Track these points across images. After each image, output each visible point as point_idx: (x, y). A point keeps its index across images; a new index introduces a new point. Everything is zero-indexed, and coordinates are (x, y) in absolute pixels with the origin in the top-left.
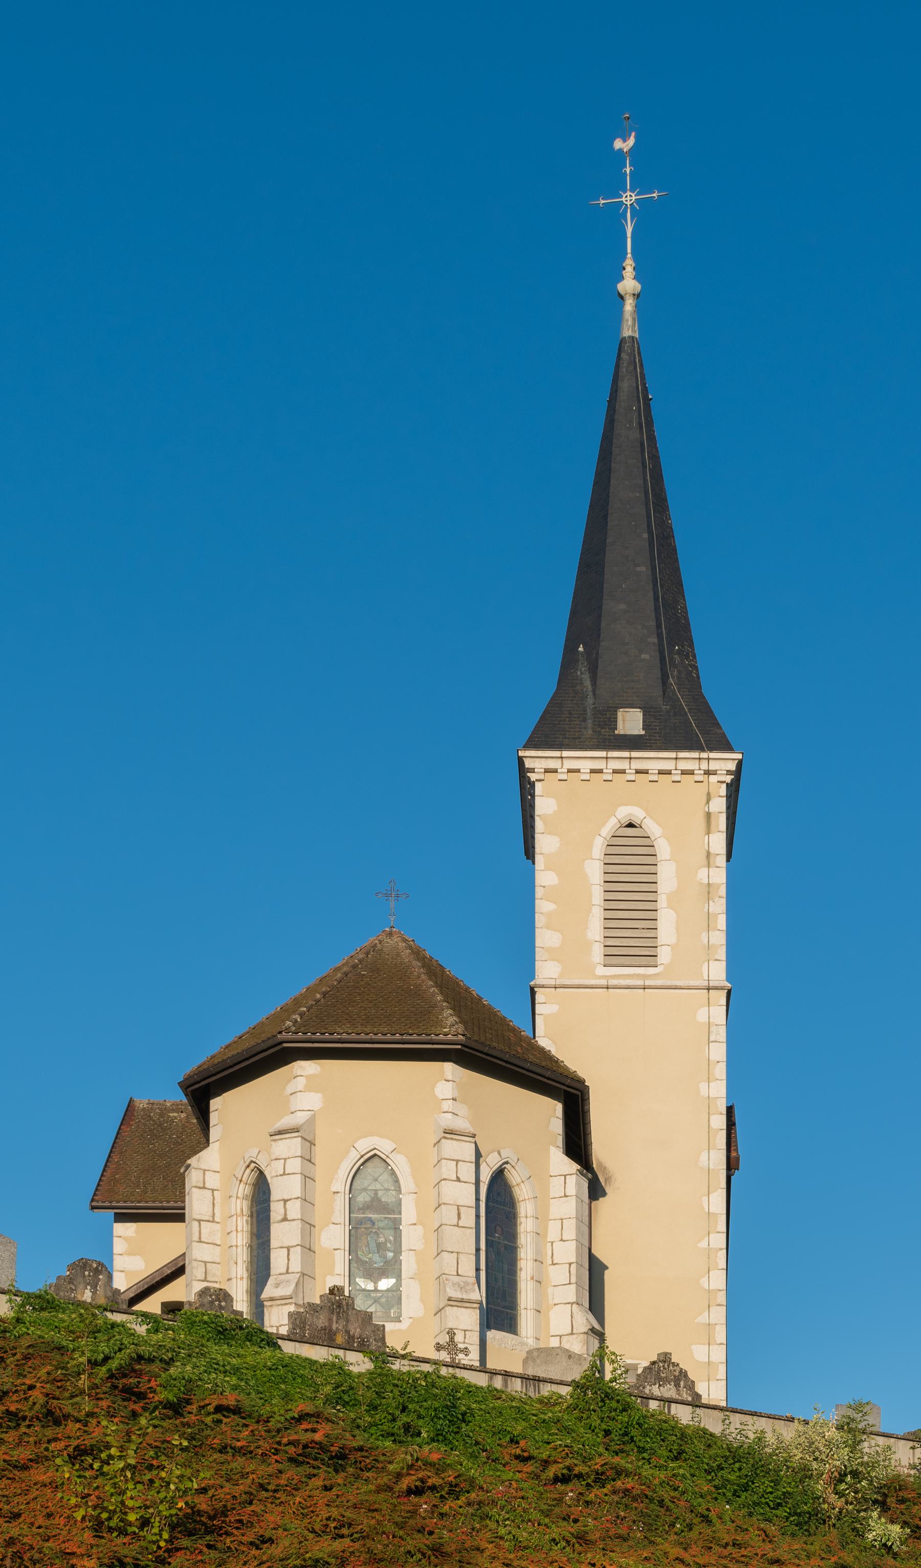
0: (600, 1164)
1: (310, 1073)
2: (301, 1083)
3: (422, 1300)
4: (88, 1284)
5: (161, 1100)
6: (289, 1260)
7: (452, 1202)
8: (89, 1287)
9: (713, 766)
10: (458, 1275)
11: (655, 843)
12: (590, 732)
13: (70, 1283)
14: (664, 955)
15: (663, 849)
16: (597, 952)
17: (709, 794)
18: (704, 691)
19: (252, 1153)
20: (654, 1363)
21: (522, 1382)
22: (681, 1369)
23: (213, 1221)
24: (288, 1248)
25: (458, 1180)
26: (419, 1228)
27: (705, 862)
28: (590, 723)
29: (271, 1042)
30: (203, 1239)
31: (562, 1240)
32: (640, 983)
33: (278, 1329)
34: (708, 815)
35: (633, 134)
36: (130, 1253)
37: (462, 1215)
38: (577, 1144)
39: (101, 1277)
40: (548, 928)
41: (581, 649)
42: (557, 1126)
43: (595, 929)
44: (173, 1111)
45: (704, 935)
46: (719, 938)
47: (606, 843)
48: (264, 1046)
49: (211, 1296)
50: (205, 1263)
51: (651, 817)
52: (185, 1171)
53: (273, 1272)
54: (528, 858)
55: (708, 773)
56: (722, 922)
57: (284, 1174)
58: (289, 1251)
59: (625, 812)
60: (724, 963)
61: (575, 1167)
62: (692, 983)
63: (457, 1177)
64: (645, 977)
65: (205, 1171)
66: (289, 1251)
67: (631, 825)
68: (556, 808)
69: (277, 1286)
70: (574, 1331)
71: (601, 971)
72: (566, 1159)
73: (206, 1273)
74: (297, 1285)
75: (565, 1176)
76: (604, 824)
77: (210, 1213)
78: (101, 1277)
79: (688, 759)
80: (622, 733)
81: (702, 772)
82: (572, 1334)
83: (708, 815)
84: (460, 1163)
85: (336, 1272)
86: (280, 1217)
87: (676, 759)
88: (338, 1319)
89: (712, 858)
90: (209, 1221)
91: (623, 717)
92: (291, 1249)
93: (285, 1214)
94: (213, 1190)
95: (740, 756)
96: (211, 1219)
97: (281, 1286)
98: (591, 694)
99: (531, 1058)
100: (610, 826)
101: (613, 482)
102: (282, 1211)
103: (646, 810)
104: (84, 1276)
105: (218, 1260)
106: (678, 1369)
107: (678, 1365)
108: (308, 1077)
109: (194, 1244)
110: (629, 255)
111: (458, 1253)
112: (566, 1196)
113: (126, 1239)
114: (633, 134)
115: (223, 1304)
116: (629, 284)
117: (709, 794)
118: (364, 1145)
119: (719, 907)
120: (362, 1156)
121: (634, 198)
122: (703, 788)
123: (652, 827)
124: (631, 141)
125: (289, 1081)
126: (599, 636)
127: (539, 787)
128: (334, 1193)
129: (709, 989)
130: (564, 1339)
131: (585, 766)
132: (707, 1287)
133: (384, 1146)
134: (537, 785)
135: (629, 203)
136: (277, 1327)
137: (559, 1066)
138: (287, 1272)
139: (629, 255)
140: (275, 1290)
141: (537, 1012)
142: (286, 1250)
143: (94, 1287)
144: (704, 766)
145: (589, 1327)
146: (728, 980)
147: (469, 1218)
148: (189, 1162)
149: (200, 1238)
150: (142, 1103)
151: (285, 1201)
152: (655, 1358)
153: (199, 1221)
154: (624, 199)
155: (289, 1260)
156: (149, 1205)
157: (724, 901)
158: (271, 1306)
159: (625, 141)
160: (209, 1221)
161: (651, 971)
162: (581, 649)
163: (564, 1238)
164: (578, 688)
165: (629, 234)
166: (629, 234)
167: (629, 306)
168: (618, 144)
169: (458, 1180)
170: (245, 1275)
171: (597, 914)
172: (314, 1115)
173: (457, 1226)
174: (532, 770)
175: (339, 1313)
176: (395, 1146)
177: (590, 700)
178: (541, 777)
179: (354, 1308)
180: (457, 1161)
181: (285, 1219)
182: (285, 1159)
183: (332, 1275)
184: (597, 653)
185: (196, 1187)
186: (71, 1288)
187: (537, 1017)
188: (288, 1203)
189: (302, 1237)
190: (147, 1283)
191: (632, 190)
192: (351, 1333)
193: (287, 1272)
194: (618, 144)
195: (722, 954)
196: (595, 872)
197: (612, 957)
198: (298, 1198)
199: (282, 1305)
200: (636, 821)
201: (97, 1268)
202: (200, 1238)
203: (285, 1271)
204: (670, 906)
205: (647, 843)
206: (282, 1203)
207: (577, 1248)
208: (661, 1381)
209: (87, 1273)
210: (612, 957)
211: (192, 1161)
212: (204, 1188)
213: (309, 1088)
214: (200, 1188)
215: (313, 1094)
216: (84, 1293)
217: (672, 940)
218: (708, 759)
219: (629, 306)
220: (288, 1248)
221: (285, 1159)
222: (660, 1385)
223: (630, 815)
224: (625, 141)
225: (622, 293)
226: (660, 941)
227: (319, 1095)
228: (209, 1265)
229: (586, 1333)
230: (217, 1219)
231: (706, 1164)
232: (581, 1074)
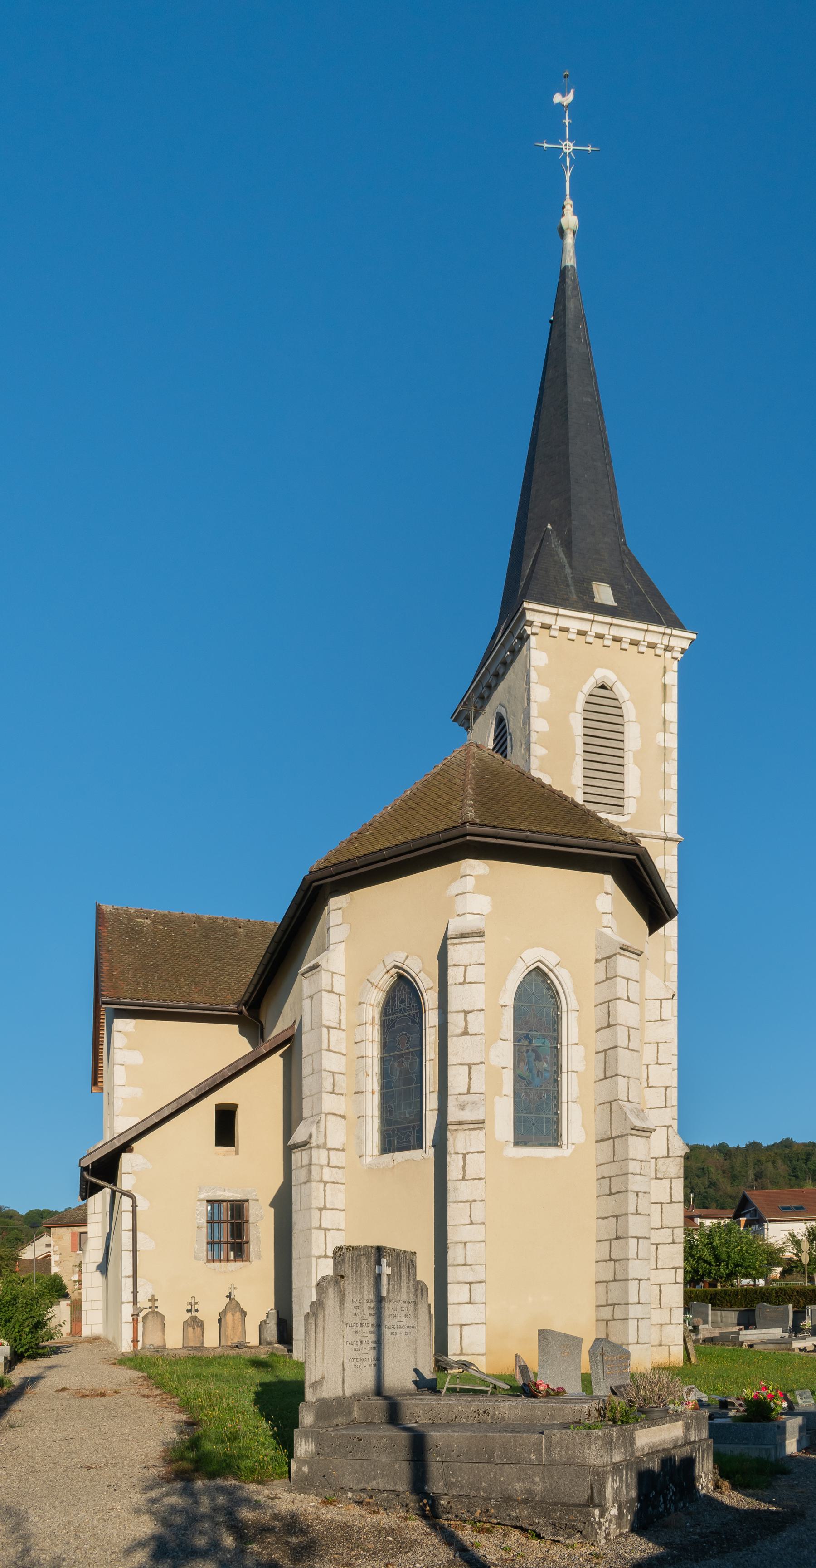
1: (480, 873)
2: (470, 883)
3: (583, 1126)
5: (124, 907)
6: (470, 1078)
9: (674, 642)
10: (629, 1101)
11: (623, 706)
12: (575, 596)
14: (631, 806)
15: (629, 711)
17: (665, 667)
24: (470, 1066)
25: (628, 1000)
26: (581, 1048)
27: (662, 728)
28: (572, 588)
29: (455, 833)
30: (331, 1048)
31: (657, 1063)
34: (665, 686)
35: (572, 91)
36: (130, 1048)
41: (549, 526)
44: (139, 917)
45: (661, 792)
46: (672, 796)
48: (432, 840)
50: (333, 1073)
55: (667, 648)
56: (674, 782)
57: (464, 982)
58: (470, 1068)
59: (602, 674)
60: (676, 818)
62: (654, 833)
65: (333, 973)
66: (470, 1068)
67: (603, 687)
70: (671, 1154)
75: (661, 1000)
76: (584, 682)
77: (337, 1020)
79: (655, 633)
82: (668, 1157)
83: (665, 686)
84: (630, 982)
85: (504, 1093)
87: (646, 631)
89: (667, 723)
92: (474, 1067)
93: (466, 1027)
94: (340, 995)
95: (694, 636)
96: (338, 1026)
98: (567, 566)
100: (589, 686)
101: (569, 385)
102: (463, 1024)
103: (617, 675)
105: (344, 1072)
108: (478, 878)
109: (324, 1053)
110: (568, 196)
112: (661, 1020)
113: (127, 1034)
114: (572, 91)
116: (570, 220)
117: (665, 667)
118: (531, 957)
119: (672, 767)
120: (551, 970)
121: (572, 148)
122: (659, 662)
123: (621, 691)
124: (570, 97)
125: (454, 880)
126: (570, 515)
127: (533, 639)
128: (502, 1006)
129: (665, 840)
130: (660, 1162)
131: (574, 626)
133: (550, 959)
134: (532, 638)
135: (568, 151)
138: (469, 1093)
139: (568, 196)
140: (462, 1113)
142: (466, 1068)
144: (666, 642)
146: (679, 833)
150: (108, 908)
151: (466, 1013)
153: (328, 1028)
154: (564, 147)
155: (470, 1078)
156: (155, 1000)
157: (676, 763)
158: (456, 1130)
159: (564, 96)
162: (549, 526)
163: (660, 1062)
164: (556, 557)
165: (568, 178)
166: (568, 178)
167: (570, 240)
168: (557, 98)
169: (628, 1000)
170: (377, 1088)
171: (579, 763)
174: (531, 624)
177: (568, 570)
178: (535, 630)
181: (465, 1033)
182: (466, 966)
183: (500, 1096)
184: (570, 530)
185: (326, 991)
188: (469, 1015)
190: (208, 1085)
191: (570, 140)
193: (469, 1093)
194: (557, 98)
195: (674, 810)
199: (470, 1130)
200: (609, 684)
203: (465, 1091)
204: (635, 763)
205: (615, 704)
206: (462, 1015)
213: (478, 890)
214: (329, 992)
215: (482, 896)
217: (637, 794)
219: (570, 240)
220: (470, 1066)
221: (466, 966)
223: (604, 677)
224: (564, 96)
225: (564, 226)
227: (488, 898)
228: (336, 1075)
230: (343, 1027)
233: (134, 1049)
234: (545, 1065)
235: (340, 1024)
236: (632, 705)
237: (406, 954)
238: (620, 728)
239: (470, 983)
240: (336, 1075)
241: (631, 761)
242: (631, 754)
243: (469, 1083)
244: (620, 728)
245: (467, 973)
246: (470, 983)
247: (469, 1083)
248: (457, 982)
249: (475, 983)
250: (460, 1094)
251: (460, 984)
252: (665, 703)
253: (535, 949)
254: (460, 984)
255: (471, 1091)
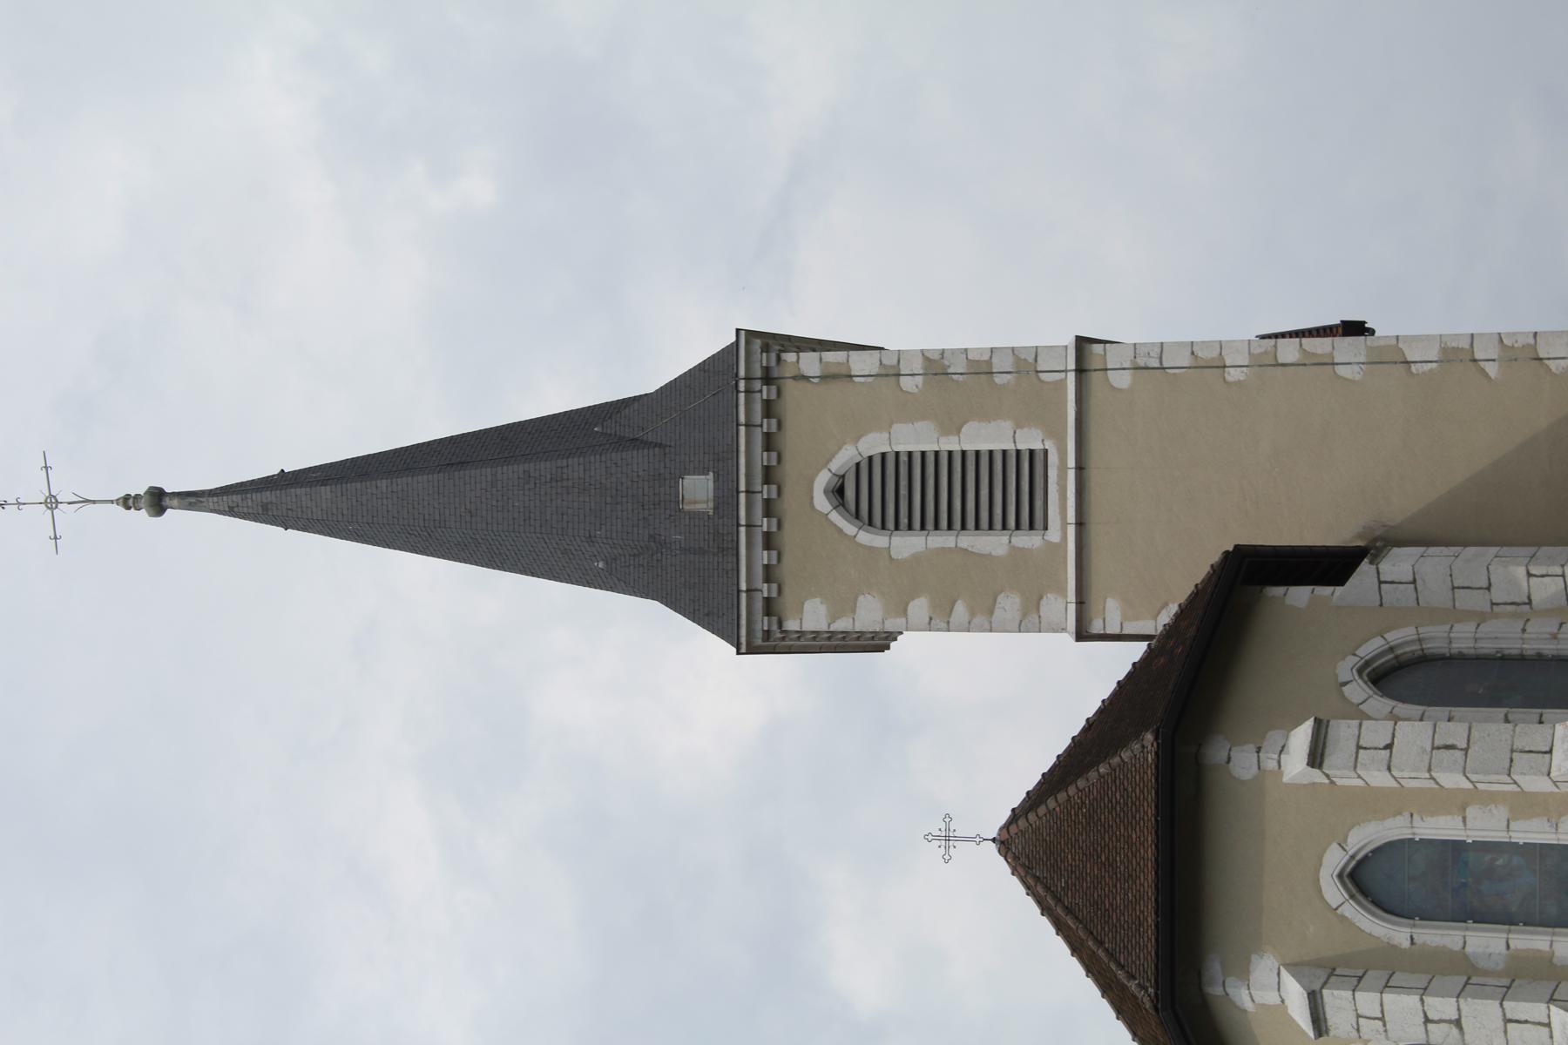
6: (1526, 1022)
11: (866, 454)
15: (874, 444)
24: (1508, 1021)
25: (1389, 747)
31: (1489, 588)
57: (1382, 1019)
75: (1380, 582)
83: (825, 378)
84: (1362, 743)
93: (1450, 1022)
133: (1335, 859)
151: (1427, 1020)
155: (1526, 1022)
163: (1485, 585)
169: (1389, 747)
182: (1359, 1016)
188: (1430, 1016)
203: (1546, 1030)
221: (1359, 1016)
223: (826, 492)
237: (1335, 845)
238: (904, 458)
242: (943, 440)
244: (904, 458)
248: (1382, 1029)
253: (1322, 882)
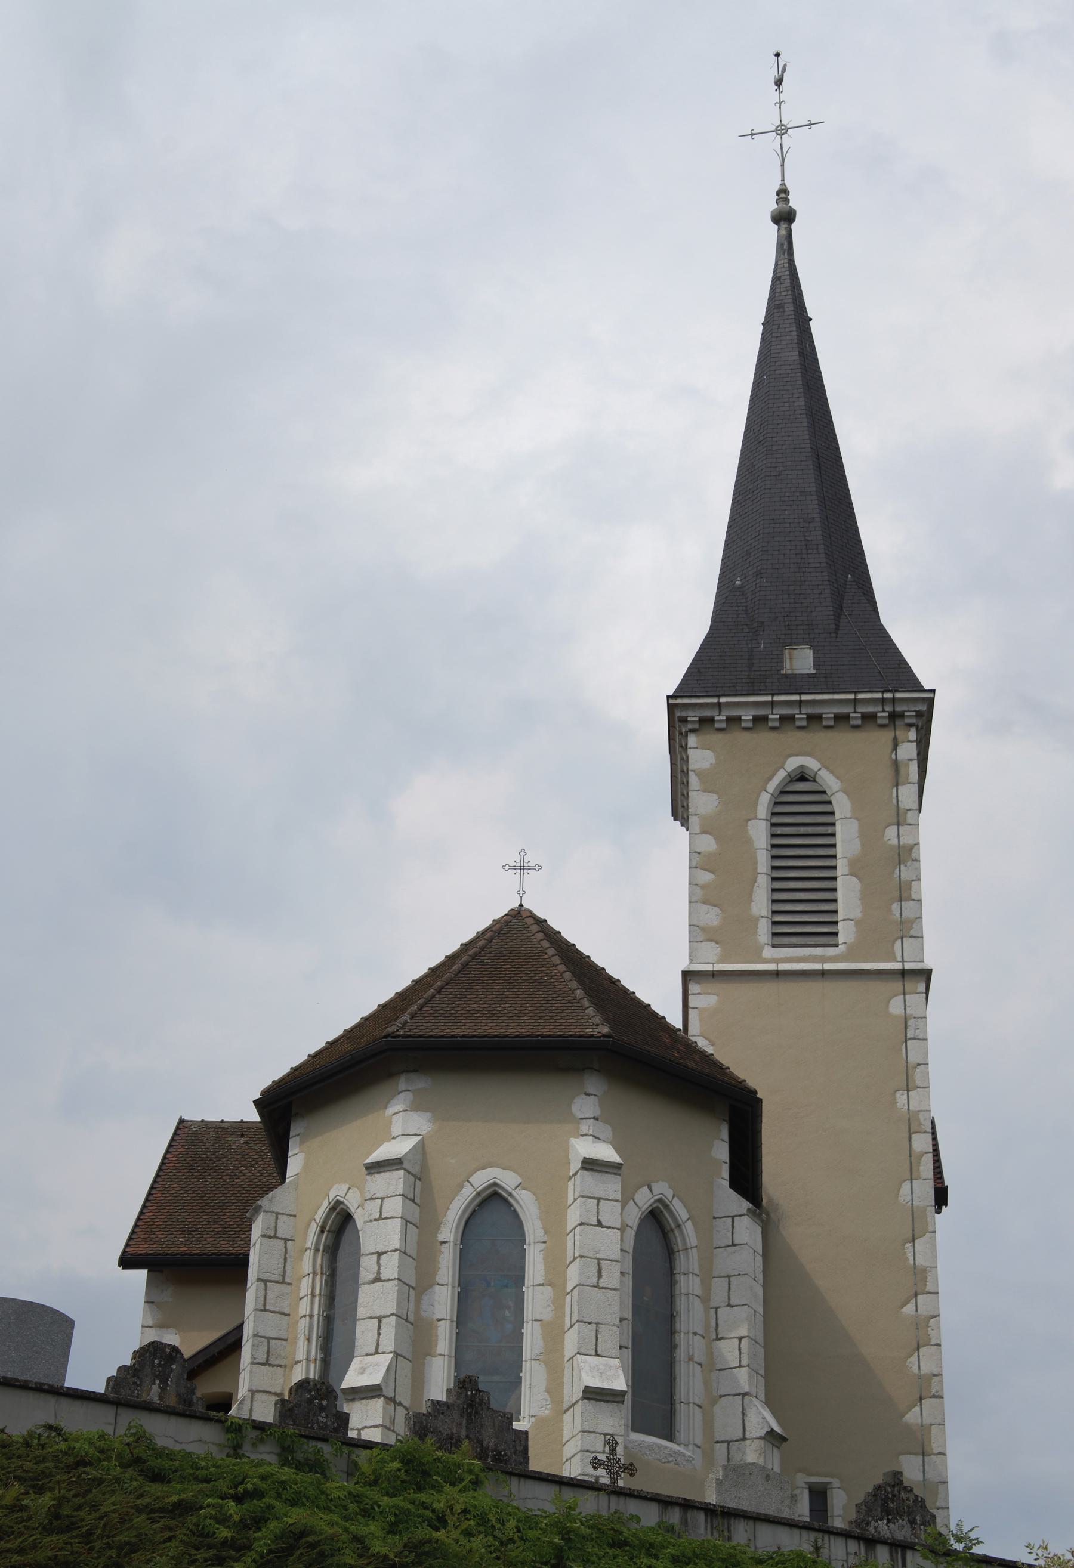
0: (770, 1200)
3: (548, 1391)
4: (157, 1377)
6: (379, 1334)
7: (590, 1254)
8: (157, 1382)
10: (597, 1355)
11: (833, 799)
13: (134, 1376)
14: (846, 932)
15: (842, 805)
16: (764, 930)
18: (885, 620)
19: (338, 1191)
20: (879, 1487)
21: (706, 1516)
22: (917, 1496)
23: (283, 1282)
25: (599, 1224)
31: (729, 1305)
32: (817, 966)
33: (359, 1434)
37: (604, 1273)
38: (746, 1177)
39: (174, 1367)
40: (704, 902)
42: (721, 1152)
43: (761, 904)
47: (774, 800)
49: (310, 1391)
50: (269, 1339)
51: (828, 769)
52: (253, 1215)
53: (358, 1350)
54: (675, 819)
57: (380, 1218)
58: (380, 1322)
61: (745, 1205)
63: (599, 1221)
64: (823, 959)
65: (278, 1214)
66: (380, 1322)
68: (713, 761)
69: (363, 1371)
70: (748, 1435)
71: (768, 952)
72: (734, 1195)
73: (268, 1353)
74: (388, 1370)
75: (733, 1217)
78: (174, 1367)
80: (789, 672)
81: (886, 714)
83: (896, 764)
84: (602, 1202)
86: (371, 1277)
88: (468, 1423)
90: (277, 1282)
91: (790, 655)
92: (384, 1320)
93: (379, 1273)
94: (286, 1240)
97: (367, 1372)
99: (691, 1064)
104: (153, 1365)
106: (912, 1498)
107: (911, 1490)
111: (597, 1324)
115: (324, 1403)
118: (481, 1179)
123: (829, 781)
130: (734, 1446)
132: (916, 1371)
133: (508, 1180)
136: (359, 1430)
137: (726, 1074)
138: (377, 1353)
141: (691, 1004)
143: (164, 1381)
145: (767, 1429)
147: (612, 1277)
148: (259, 1202)
149: (265, 1305)
151: (380, 1254)
152: (879, 1481)
155: (379, 1334)
160: (277, 1282)
161: (831, 951)
163: (732, 1302)
169: (599, 1224)
172: (423, 1140)
173: (597, 1286)
175: (470, 1413)
176: (519, 1180)
179: (489, 1408)
180: (599, 1199)
181: (378, 1279)
182: (383, 1199)
186: (134, 1383)
187: (690, 1011)
188: (383, 1257)
189: (398, 1304)
192: (485, 1444)
196: (759, 833)
197: (780, 936)
198: (395, 1250)
201: (170, 1354)
202: (265, 1305)
203: (373, 1351)
206: (375, 1257)
207: (399, 1293)
208: (889, 1515)
209: (157, 1361)
210: (780, 936)
211: (264, 1202)
212: (275, 1237)
216: (150, 1389)
217: (857, 914)
218: (894, 699)
220: (380, 1319)
221: (383, 1199)
222: (889, 1521)
223: (802, 766)
226: (841, 916)
228: (273, 1342)
229: (761, 1438)
231: (909, 1198)
232: (752, 1083)
233: (168, 1327)
234: (507, 1313)
235: (284, 1276)
236: (846, 797)
239: (386, 1218)
240: (273, 1342)
241: (846, 871)
243: (378, 1340)
245: (384, 1206)
246: (386, 1218)
247: (378, 1340)
248: (372, 1218)
249: (392, 1218)
250: (367, 1355)
251: (376, 1220)
252: (897, 786)
254: (376, 1220)
255: (380, 1351)
